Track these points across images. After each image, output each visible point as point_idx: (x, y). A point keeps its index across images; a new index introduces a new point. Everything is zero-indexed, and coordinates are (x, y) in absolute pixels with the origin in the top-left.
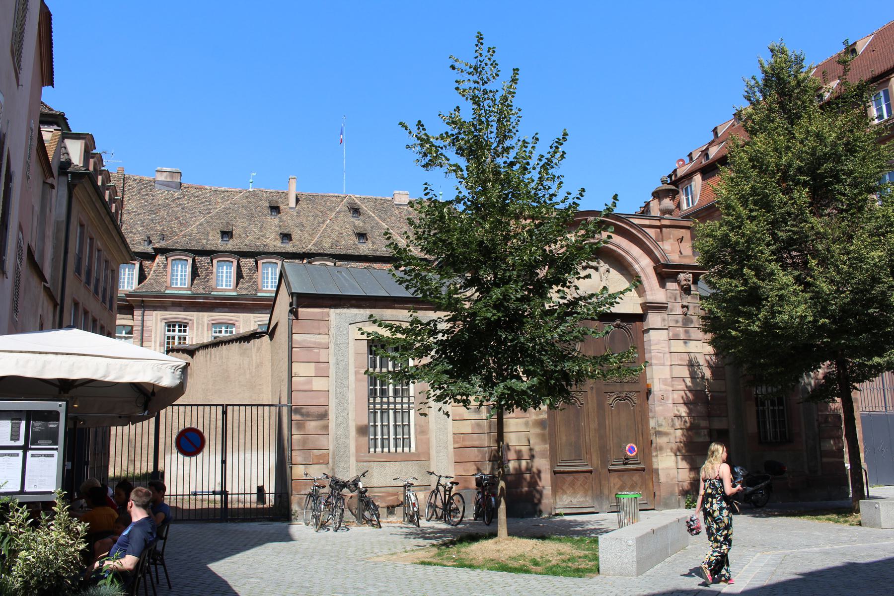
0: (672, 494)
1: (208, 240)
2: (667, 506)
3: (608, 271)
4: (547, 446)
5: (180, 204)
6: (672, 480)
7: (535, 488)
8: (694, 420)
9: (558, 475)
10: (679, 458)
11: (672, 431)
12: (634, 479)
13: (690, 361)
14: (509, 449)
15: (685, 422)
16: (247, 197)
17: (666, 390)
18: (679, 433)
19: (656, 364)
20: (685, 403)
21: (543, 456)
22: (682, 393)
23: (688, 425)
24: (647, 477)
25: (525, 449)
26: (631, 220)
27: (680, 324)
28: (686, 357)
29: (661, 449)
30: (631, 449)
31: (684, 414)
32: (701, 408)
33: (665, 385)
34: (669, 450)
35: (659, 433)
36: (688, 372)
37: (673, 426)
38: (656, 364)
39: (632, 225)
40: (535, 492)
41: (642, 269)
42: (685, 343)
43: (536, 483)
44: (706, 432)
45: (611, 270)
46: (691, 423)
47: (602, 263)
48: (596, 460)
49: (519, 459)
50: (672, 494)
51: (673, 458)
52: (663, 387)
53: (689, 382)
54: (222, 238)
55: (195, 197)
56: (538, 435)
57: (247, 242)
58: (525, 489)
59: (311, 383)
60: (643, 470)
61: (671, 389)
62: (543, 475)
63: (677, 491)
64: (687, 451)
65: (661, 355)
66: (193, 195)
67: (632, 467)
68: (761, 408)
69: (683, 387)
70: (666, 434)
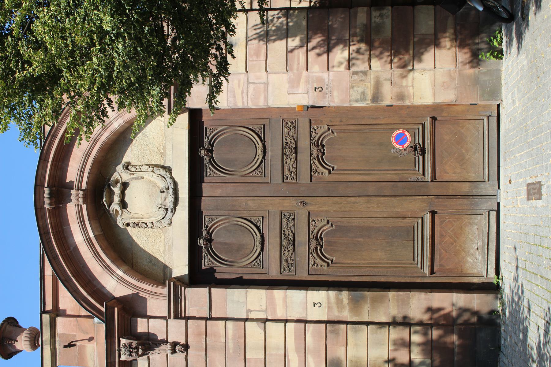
0: (476, 81)
2: (494, 91)
3: (127, 167)
6: (452, 78)
7: (454, 320)
8: (355, 35)
9: (436, 269)
10: (417, 66)
11: (372, 76)
13: (260, 37)
14: (393, 360)
15: (358, 51)
17: (307, 82)
18: (376, 64)
19: (266, 99)
20: (328, 51)
21: (405, 303)
22: (312, 54)
23: (363, 46)
24: (445, 114)
25: (396, 333)
28: (254, 43)
29: (401, 97)
30: (400, 139)
31: (346, 54)
32: (336, 20)
33: (299, 82)
34: (404, 82)
35: (376, 98)
36: (278, 43)
37: (365, 73)
38: (266, 99)
40: (460, 321)
41: (112, 272)
43: (447, 316)
44: (375, 14)
45: (125, 160)
46: (360, 41)
47: (116, 176)
49: (408, 345)
50: (476, 81)
51: (416, 74)
52: (302, 88)
53: (294, 42)
56: (373, 308)
58: (454, 338)
60: (434, 119)
61: (305, 73)
62: (435, 305)
63: (472, 71)
64: (407, 51)
65: (251, 87)
67: (428, 141)
69: (301, 54)
70: (378, 86)
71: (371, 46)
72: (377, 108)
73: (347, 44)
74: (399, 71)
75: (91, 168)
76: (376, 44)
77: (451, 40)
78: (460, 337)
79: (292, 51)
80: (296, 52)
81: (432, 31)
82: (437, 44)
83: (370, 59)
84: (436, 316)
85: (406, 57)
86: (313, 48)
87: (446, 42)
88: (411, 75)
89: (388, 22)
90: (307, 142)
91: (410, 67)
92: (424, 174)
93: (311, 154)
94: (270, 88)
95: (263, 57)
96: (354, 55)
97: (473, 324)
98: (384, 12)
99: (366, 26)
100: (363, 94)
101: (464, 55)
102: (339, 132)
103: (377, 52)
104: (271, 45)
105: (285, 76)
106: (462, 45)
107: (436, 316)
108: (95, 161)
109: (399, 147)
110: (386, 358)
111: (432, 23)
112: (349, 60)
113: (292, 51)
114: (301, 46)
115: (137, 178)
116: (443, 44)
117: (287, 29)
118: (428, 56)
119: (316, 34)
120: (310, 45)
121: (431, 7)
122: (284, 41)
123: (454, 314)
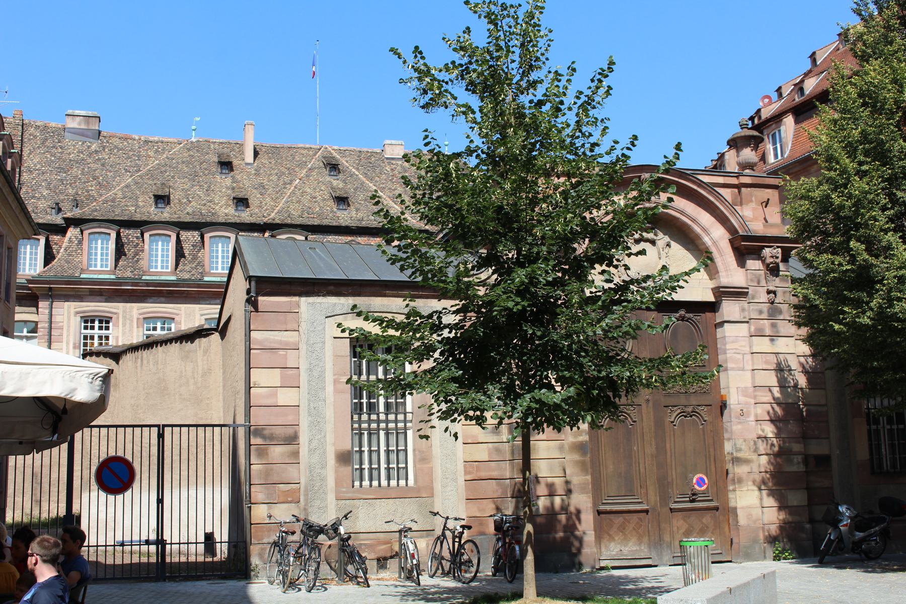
0: (755, 541)
1: (137, 206)
3: (668, 245)
4: (589, 477)
5: (99, 159)
6: (755, 522)
8: (784, 442)
10: (764, 493)
11: (754, 457)
12: (704, 521)
13: (779, 364)
14: (538, 482)
15: (772, 445)
16: (189, 150)
17: (747, 403)
18: (764, 459)
19: (733, 369)
20: (771, 421)
21: (583, 490)
22: (768, 407)
23: (776, 449)
24: (721, 518)
26: (700, 177)
27: (765, 316)
28: (773, 359)
29: (740, 481)
30: (700, 482)
31: (770, 435)
32: (793, 427)
33: (746, 396)
34: (750, 483)
35: (737, 461)
36: (775, 379)
38: (733, 369)
39: (701, 184)
40: (572, 539)
42: (772, 340)
43: (575, 528)
45: (673, 243)
46: (779, 445)
47: (661, 235)
48: (653, 497)
49: (551, 494)
50: (755, 541)
52: (743, 399)
53: (777, 392)
54: (156, 204)
55: (119, 150)
57: (189, 210)
59: (275, 395)
60: (717, 509)
61: (753, 401)
62: (583, 516)
63: (761, 537)
64: (775, 484)
65: (740, 356)
66: (116, 147)
67: (701, 505)
68: (874, 427)
69: (769, 398)
70: (747, 461)
71: (777, 455)
72: (723, 461)
73: (778, 436)
74: (758, 478)
75: (671, 215)
76: (778, 460)
77: (784, 520)
78: (561, 538)
79: (770, 390)
80: (770, 394)
81: (790, 504)
82: (780, 508)
83: (767, 454)
84: (574, 517)
85: (770, 484)
86: (773, 408)
87: (782, 516)
88: (755, 488)
89: (794, 469)
90: (694, 403)
91: (763, 487)
92: (603, 504)
93: (685, 406)
94: (740, 372)
95: (765, 367)
96: (770, 442)
97: (571, 550)
98: (802, 466)
99: (791, 451)
100: (740, 450)
101: (774, 530)
102: (703, 429)
103: (772, 460)
104: (773, 373)
105: (749, 385)
106: (781, 528)
107: (574, 517)
108: (677, 219)
109: (694, 481)
110: (539, 475)
111: (795, 504)
112: (765, 438)
113: (770, 390)
114: (774, 398)
115: (659, 254)
116: (781, 513)
117: (785, 387)
118: (770, 502)
119: (784, 410)
120: (775, 406)
121: (806, 503)
122: (777, 384)
123: (577, 533)
